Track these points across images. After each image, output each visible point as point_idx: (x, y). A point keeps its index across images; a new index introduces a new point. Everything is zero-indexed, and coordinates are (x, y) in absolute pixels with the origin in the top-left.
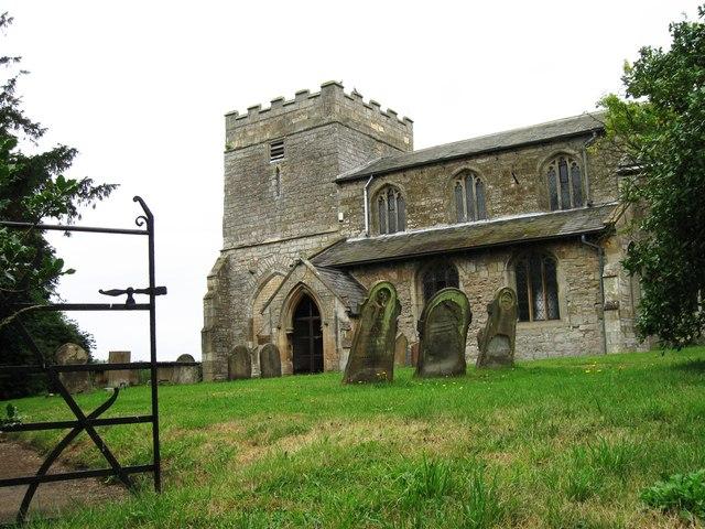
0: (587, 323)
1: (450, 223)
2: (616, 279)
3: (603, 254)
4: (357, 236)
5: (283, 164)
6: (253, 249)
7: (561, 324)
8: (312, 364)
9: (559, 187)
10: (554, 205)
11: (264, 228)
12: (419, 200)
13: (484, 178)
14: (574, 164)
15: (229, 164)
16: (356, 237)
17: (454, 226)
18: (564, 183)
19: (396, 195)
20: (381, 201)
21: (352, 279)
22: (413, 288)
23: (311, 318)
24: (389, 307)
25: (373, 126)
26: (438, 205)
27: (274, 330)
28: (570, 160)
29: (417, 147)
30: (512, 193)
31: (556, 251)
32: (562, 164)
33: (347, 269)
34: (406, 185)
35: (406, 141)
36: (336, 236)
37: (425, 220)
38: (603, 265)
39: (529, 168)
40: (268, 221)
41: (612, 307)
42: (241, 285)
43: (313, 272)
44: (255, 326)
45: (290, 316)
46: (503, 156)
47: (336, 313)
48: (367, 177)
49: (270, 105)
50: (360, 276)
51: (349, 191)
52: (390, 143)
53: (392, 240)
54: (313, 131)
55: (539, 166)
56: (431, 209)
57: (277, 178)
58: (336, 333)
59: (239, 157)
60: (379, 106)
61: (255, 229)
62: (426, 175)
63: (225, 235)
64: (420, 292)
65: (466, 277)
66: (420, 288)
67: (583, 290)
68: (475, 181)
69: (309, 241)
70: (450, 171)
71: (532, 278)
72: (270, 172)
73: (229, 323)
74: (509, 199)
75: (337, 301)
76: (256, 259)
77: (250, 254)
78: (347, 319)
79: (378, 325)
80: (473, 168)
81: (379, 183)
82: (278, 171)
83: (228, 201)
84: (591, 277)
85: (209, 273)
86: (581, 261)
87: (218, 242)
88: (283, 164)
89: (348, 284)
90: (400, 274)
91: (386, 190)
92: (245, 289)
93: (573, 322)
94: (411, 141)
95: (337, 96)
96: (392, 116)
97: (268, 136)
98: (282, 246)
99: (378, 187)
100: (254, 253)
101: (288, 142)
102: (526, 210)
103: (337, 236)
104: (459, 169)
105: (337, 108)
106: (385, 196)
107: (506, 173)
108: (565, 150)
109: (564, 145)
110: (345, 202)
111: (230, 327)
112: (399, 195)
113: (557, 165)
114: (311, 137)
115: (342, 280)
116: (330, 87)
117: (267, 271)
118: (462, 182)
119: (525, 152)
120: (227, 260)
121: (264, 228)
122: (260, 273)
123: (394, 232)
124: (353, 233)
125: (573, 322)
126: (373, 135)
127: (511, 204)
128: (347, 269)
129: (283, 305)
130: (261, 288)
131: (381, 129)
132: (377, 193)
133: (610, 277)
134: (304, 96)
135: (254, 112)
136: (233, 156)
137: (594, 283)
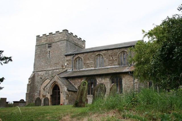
4: (70, 70)
17: (95, 68)
19: (81, 60)
21: (68, 81)
23: (57, 91)
26: (92, 63)
27: (47, 94)
31: (122, 76)
34: (83, 57)
39: (115, 54)
45: (52, 90)
46: (109, 51)
50: (71, 80)
56: (90, 64)
57: (49, 53)
60: (77, 36)
62: (89, 55)
74: (110, 62)
80: (101, 54)
81: (77, 56)
82: (50, 51)
86: (128, 79)
89: (68, 82)
91: (78, 58)
94: (85, 46)
99: (76, 57)
102: (114, 65)
104: (97, 54)
106: (78, 60)
107: (110, 56)
109: (125, 49)
110: (67, 61)
112: (82, 59)
115: (66, 81)
119: (115, 50)
120: (35, 74)
128: (67, 78)
132: (76, 59)
135: (44, 36)
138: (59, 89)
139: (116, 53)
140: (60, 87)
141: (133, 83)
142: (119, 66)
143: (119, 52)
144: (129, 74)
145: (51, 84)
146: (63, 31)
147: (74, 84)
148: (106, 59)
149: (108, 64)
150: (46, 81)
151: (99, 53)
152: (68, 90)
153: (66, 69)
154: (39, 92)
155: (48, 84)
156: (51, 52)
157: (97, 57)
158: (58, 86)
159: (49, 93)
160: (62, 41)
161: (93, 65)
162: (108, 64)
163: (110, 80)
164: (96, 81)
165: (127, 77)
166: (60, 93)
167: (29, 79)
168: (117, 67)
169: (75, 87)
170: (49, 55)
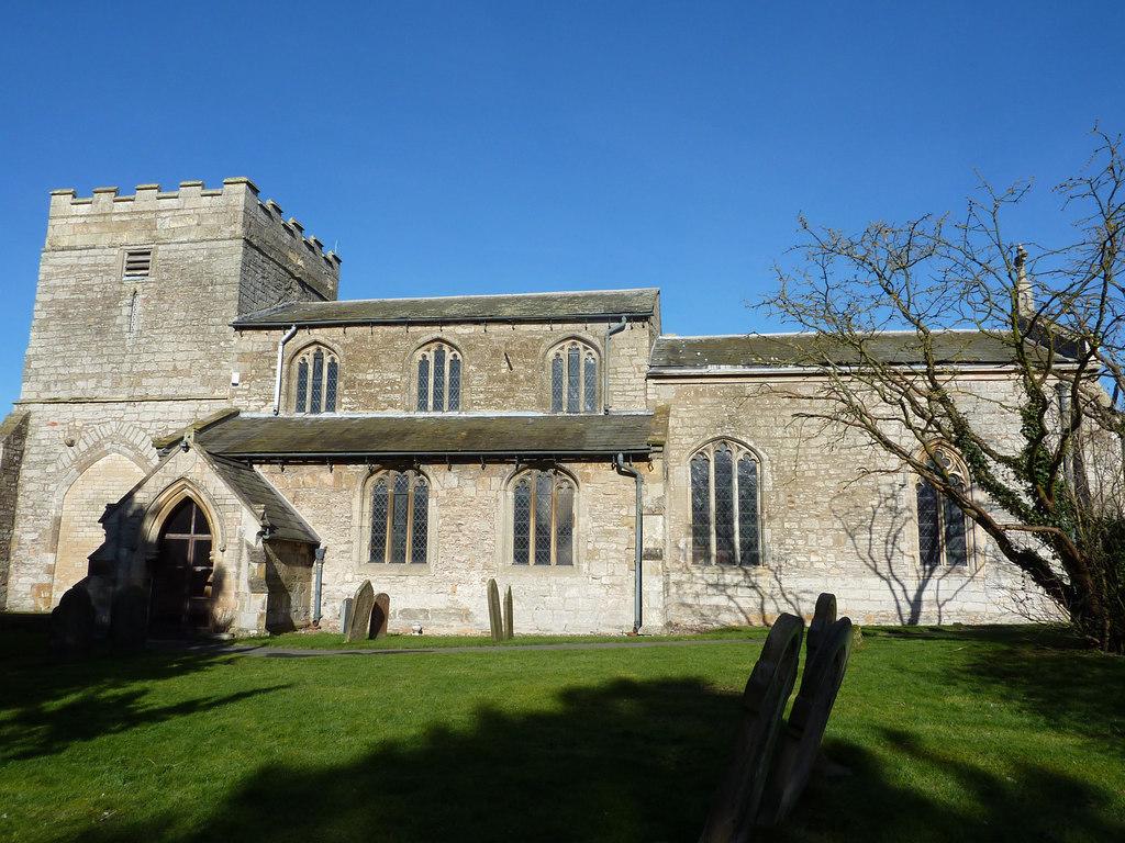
11: (100, 377)
12: (364, 371)
22: (356, 502)
23: (192, 537)
25: (291, 255)
26: (392, 383)
27: (124, 552)
30: (502, 381)
36: (658, 439)
39: (530, 349)
40: (108, 368)
41: (656, 555)
47: (241, 534)
51: (256, 341)
54: (205, 245)
55: (542, 350)
61: (84, 376)
65: (442, 494)
69: (178, 406)
74: (496, 387)
81: (304, 337)
91: (434, 347)
92: (51, 469)
93: (593, 571)
97: (125, 238)
101: (161, 252)
102: (518, 406)
103: (224, 406)
104: (428, 338)
107: (495, 353)
110: (243, 356)
121: (100, 377)
122: (83, 446)
131: (300, 263)
137: (626, 521)
138: (204, 526)
139: (533, 340)
143: (551, 342)
147: (291, 495)
149: (482, 396)
154: (48, 525)
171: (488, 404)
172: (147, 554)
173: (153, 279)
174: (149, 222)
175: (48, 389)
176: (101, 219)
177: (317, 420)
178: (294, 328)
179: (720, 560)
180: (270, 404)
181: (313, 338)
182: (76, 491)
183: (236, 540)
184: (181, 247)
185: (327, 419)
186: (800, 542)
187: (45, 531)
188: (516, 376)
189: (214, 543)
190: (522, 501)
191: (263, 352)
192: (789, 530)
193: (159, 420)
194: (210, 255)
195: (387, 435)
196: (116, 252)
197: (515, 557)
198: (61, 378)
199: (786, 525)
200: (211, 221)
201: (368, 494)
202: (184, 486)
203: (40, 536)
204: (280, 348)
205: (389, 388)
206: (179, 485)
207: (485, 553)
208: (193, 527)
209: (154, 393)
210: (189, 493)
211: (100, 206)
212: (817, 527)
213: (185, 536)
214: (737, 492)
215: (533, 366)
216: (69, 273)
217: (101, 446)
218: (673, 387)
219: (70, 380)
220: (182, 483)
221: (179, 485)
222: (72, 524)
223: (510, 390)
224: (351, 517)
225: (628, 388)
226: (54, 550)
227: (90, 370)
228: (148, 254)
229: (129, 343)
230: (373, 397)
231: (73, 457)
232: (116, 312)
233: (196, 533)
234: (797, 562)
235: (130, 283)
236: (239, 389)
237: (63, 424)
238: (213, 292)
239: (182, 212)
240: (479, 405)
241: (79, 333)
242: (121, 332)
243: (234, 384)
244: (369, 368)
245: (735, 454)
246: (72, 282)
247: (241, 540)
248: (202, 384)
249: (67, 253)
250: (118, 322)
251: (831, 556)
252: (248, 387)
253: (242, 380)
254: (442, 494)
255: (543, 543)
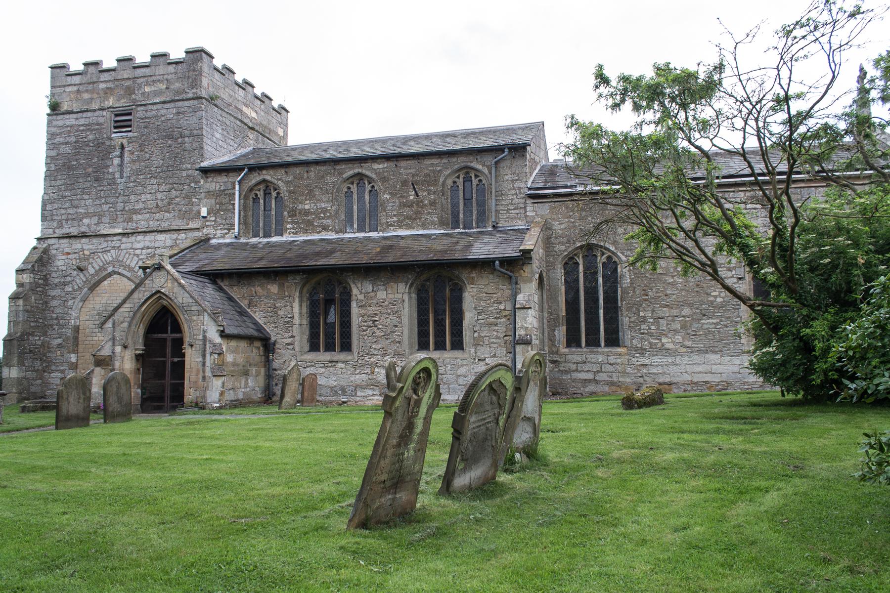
0: (494, 356)
1: (337, 232)
2: (529, 310)
3: (516, 283)
4: (223, 237)
5: (130, 140)
6: (84, 240)
7: (466, 356)
8: (168, 393)
9: (461, 204)
10: (456, 225)
11: (100, 215)
13: (379, 186)
14: (480, 181)
15: (53, 130)
16: (222, 238)
17: (341, 236)
18: (467, 201)
19: (274, 194)
20: (256, 199)
21: (221, 289)
22: (296, 305)
23: (170, 336)
24: (427, 397)
25: (245, 110)
26: (324, 211)
27: (118, 349)
28: (476, 176)
29: (293, 140)
30: (411, 206)
31: (464, 275)
32: (468, 179)
33: (214, 277)
34: (287, 183)
35: (281, 132)
36: (197, 234)
37: (308, 227)
38: (515, 295)
39: (431, 180)
40: (105, 207)
42: (65, 284)
43: (176, 280)
44: (80, 335)
45: (141, 331)
46: (403, 163)
47: (204, 332)
48: (239, 169)
49: (82, 68)
50: (231, 286)
51: (215, 184)
52: (263, 132)
53: (266, 245)
54: (172, 105)
55: (442, 179)
56: (316, 214)
57: (121, 156)
58: (204, 356)
59: (68, 123)
60: (253, 87)
61: (87, 215)
62: (312, 174)
63: (44, 218)
64: (305, 310)
65: (361, 297)
66: (304, 305)
67: (491, 320)
68: (368, 187)
69: (161, 237)
70: (341, 174)
71: (436, 303)
72: (112, 148)
73: (44, 329)
74: (407, 211)
75: (206, 317)
76: (87, 253)
77: (79, 246)
78: (218, 340)
79: (410, 426)
80: (368, 173)
81: (255, 178)
82: (122, 147)
83: (50, 177)
84: (502, 307)
85: (18, 263)
86: (491, 288)
87: (35, 228)
88: (130, 140)
89: (217, 295)
90: (282, 286)
91: (262, 187)
92: (69, 289)
94: (286, 133)
95: (205, 68)
96: (266, 100)
97: (110, 102)
98: (124, 239)
99: (254, 182)
100: (86, 245)
101: (140, 112)
102: (424, 226)
104: (351, 173)
105: (205, 82)
106: (261, 194)
107: (404, 183)
108: (472, 165)
109: (471, 158)
110: (210, 194)
111: (45, 334)
112: (278, 193)
113: (461, 179)
114: (169, 112)
115: (210, 290)
116: (197, 54)
117: (102, 269)
118: (354, 188)
119: (428, 162)
120: (46, 251)
121: (100, 215)
122: (91, 271)
123: (270, 236)
124: (219, 233)
125: (479, 354)
126: (246, 121)
127: (407, 217)
128: (214, 277)
129: (133, 318)
130: (92, 288)
131: (254, 115)
132: (251, 189)
133: (524, 308)
134: (161, 59)
135: (92, 69)
136: (61, 121)
137: (504, 313)
139: (434, 172)
140: (182, 318)
141: (509, 306)
142: (442, 231)
144: (495, 270)
145: (137, 305)
146: (153, 56)
147: (246, 302)
148: (388, 197)
149: (395, 219)
150: (106, 282)
151: (356, 171)
152: (223, 331)
153: (205, 231)
154: (69, 333)
155: (124, 301)
156: (127, 149)
157: (349, 188)
158: (172, 315)
159: (125, 347)
160: (183, 100)
161: (329, 222)
162: (395, 219)
163: (409, 293)
164: (351, 290)
165: (484, 281)
166: (186, 346)
167: (19, 271)
168: (437, 235)
169: (250, 317)
170: (121, 165)
171: (400, 225)
172: (136, 350)
173: (135, 134)
174: (128, 88)
175: (61, 226)
176: (90, 87)
177: (268, 243)
178: (246, 170)
179: (588, 344)
180: (232, 231)
181: (261, 177)
182: (89, 305)
183: (201, 337)
184: (155, 107)
185: (276, 242)
186: (653, 327)
187: (67, 338)
188: (422, 201)
189: (184, 339)
190: (423, 301)
191: (224, 190)
192: (644, 317)
193: (148, 248)
194: (178, 113)
195: (318, 254)
196: (105, 113)
197: (419, 344)
198: (70, 216)
199: (642, 314)
200: (177, 85)
201: (305, 299)
202: (160, 298)
203: (64, 341)
204: (237, 187)
205: (322, 215)
206: (155, 297)
207: (393, 342)
208: (169, 328)
209: (143, 226)
210: (165, 303)
211: (89, 76)
212: (667, 315)
213: (164, 336)
214: (601, 288)
215: (434, 193)
216: (69, 132)
217: (106, 269)
218: (547, 204)
219: (79, 219)
220: (158, 295)
221: (155, 297)
222: (87, 331)
223: (417, 212)
224: (292, 318)
225: (511, 207)
226: (76, 351)
227: (91, 210)
228: (130, 114)
229: (121, 187)
230: (310, 223)
231: (84, 279)
232: (109, 163)
233: (171, 333)
234: (650, 343)
235: (118, 137)
236: (207, 221)
237: (75, 253)
238: (182, 143)
239: (154, 78)
240: (393, 226)
241: (81, 180)
242: (114, 178)
243: (204, 217)
244: (306, 200)
245: (599, 258)
246: (73, 139)
247: (205, 338)
248: (179, 218)
249: (67, 116)
250: (111, 170)
251: (679, 338)
252: (213, 218)
253: (209, 213)
254: (361, 297)
255: (329, 336)
